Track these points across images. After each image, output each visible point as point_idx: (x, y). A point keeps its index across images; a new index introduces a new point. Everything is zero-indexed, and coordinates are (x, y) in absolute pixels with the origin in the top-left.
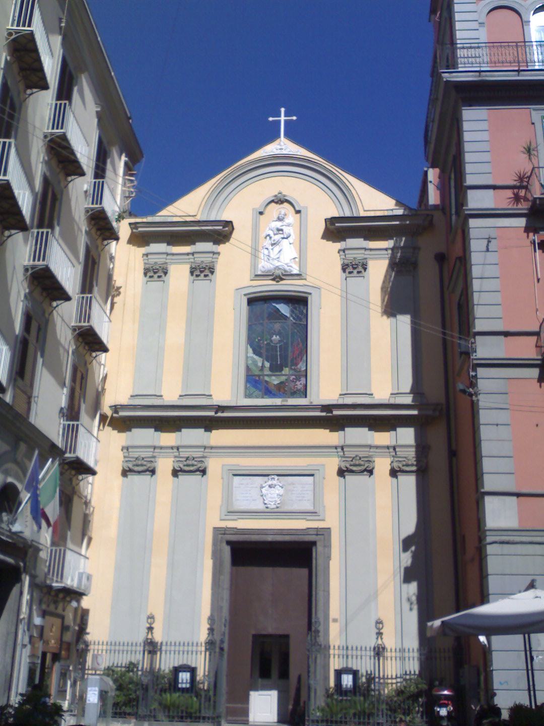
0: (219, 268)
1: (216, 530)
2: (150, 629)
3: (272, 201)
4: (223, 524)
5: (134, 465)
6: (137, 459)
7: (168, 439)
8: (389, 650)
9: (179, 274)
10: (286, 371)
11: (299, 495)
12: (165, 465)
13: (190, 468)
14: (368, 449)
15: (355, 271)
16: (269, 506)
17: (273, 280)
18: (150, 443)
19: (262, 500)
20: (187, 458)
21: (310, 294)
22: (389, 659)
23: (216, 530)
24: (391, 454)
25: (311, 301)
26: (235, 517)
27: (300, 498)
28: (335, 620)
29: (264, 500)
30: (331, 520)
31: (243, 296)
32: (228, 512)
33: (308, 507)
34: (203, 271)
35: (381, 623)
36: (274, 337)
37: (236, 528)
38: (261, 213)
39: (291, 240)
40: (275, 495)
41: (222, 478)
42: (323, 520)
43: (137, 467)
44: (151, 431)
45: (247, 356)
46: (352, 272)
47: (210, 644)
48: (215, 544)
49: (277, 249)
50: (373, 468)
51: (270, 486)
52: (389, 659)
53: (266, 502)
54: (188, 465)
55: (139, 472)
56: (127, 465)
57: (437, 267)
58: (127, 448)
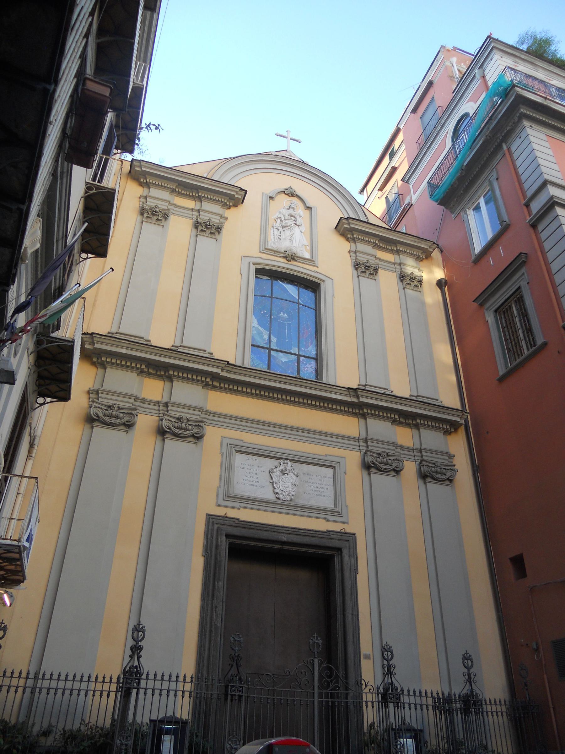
0: (224, 231)
1: (210, 518)
4: (220, 512)
6: (109, 407)
7: (153, 389)
9: (180, 228)
11: (315, 487)
12: (145, 422)
14: (394, 448)
16: (281, 496)
19: (272, 489)
20: (179, 419)
21: (324, 281)
23: (210, 518)
24: (416, 458)
25: (325, 288)
26: (237, 505)
27: (319, 493)
28: (367, 657)
29: (275, 488)
30: (356, 524)
31: (251, 264)
32: (228, 496)
33: (329, 504)
34: (208, 228)
35: (390, 650)
36: (282, 314)
37: (238, 519)
38: (271, 198)
39: (303, 228)
40: (290, 484)
41: (221, 453)
42: (347, 523)
43: (152, 214)
45: (526, 52)
46: (365, 272)
47: (199, 679)
49: (288, 233)
50: (401, 470)
53: (276, 491)
55: (111, 425)
56: (97, 411)
57: (439, 291)
58: (97, 392)
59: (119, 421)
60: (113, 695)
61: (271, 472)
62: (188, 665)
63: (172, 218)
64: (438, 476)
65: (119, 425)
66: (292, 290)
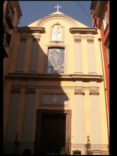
1: (38, 110)
2: (17, 138)
3: (55, 24)
4: (40, 108)
5: (78, 92)
6: (15, 89)
7: (24, 83)
8: (72, 144)
9: (84, 42)
10: (59, 66)
12: (23, 91)
13: (31, 91)
15: (23, 41)
17: (56, 43)
18: (81, 86)
20: (30, 89)
22: (72, 147)
23: (38, 110)
35: (89, 137)
38: (52, 27)
44: (81, 82)
47: (35, 143)
48: (37, 114)
51: (54, 98)
52: (72, 147)
54: (30, 91)
55: (16, 93)
58: (12, 86)
59: (32, 92)
60: (33, 146)
61: (51, 98)
62: (33, 140)
63: (28, 39)
64: (94, 93)
65: (32, 93)
66: (58, 50)
